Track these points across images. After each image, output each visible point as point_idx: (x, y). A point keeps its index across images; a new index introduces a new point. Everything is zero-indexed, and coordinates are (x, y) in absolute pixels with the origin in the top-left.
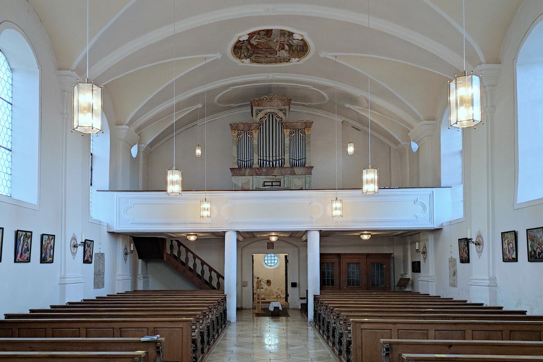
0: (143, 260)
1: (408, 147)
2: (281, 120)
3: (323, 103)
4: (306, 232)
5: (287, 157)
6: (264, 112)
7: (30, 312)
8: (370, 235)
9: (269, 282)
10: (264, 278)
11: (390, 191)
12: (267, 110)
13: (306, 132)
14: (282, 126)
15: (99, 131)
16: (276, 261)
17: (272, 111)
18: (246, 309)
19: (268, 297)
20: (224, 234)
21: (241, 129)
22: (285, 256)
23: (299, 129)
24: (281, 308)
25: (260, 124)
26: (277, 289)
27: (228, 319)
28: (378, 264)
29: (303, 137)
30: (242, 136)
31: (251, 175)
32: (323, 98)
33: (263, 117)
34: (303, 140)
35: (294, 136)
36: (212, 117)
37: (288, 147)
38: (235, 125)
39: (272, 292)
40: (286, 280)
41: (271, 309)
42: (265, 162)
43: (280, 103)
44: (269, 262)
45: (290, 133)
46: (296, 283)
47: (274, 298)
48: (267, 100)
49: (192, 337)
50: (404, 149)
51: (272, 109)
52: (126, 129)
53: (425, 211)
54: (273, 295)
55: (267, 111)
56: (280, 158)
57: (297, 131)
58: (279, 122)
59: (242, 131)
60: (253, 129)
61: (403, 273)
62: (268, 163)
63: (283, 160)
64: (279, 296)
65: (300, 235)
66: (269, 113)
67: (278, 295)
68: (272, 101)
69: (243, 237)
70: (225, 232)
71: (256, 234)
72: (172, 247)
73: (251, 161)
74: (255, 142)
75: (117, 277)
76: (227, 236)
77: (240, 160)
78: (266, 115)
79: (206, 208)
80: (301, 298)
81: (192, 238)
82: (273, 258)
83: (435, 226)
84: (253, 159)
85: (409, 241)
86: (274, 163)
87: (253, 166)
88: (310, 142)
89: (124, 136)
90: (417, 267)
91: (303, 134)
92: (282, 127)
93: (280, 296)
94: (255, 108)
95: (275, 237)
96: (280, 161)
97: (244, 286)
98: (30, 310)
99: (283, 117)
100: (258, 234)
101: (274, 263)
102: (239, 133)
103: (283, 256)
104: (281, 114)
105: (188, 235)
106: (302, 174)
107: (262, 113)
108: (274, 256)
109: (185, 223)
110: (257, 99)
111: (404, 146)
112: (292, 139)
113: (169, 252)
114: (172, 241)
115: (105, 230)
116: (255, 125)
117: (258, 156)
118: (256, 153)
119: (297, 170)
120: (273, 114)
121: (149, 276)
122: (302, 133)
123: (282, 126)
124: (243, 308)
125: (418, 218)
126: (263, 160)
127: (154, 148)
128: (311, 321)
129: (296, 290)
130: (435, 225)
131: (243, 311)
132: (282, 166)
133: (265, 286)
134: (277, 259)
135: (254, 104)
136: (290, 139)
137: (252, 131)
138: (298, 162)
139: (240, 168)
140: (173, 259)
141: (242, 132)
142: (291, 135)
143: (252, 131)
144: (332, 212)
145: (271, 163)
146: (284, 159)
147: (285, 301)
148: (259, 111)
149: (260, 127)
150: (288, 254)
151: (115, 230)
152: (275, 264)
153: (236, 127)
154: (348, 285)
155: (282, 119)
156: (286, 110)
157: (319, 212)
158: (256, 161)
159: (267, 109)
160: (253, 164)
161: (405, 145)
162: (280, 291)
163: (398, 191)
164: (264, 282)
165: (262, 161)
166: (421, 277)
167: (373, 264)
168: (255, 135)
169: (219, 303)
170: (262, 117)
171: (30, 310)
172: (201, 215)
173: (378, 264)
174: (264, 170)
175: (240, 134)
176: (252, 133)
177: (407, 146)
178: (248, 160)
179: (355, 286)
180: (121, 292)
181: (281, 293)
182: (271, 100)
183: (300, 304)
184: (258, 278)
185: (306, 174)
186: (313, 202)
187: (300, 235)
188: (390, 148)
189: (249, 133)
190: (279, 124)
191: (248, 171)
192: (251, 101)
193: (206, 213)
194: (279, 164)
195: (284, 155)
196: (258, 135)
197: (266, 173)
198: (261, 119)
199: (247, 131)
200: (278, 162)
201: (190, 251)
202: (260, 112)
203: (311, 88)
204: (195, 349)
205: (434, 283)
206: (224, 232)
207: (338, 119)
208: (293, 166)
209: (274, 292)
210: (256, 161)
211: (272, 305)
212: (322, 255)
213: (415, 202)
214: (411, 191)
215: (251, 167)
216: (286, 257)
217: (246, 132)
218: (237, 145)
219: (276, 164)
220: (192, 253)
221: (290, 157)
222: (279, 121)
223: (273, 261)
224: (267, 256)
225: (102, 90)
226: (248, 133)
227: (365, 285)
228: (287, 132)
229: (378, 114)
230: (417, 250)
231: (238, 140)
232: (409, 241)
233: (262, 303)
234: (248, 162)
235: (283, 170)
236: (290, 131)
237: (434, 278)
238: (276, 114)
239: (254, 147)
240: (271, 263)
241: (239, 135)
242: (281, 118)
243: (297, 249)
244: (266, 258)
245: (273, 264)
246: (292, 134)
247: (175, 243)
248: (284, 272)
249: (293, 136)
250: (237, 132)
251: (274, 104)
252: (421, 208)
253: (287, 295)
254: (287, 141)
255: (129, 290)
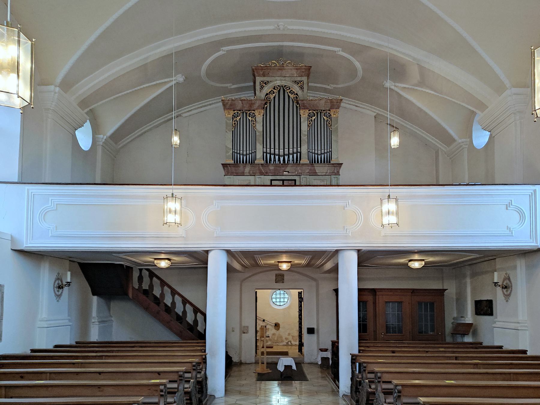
0: (102, 297)
1: (467, 146)
2: (296, 97)
3: (351, 83)
4: (337, 252)
5: (304, 149)
6: (271, 85)
7: (31, 352)
8: (424, 262)
9: (277, 326)
10: (271, 320)
11: (470, 188)
12: (276, 82)
13: (332, 114)
14: (298, 106)
15: (28, 104)
16: (286, 300)
17: (284, 83)
18: (246, 364)
19: (276, 344)
20: (206, 254)
21: (238, 108)
22: (299, 292)
23: (321, 111)
24: (294, 367)
25: (267, 101)
26: (287, 334)
27: (210, 392)
28: (426, 304)
29: (327, 121)
30: (240, 119)
31: (252, 174)
32: (353, 72)
33: (270, 92)
34: (328, 127)
35: (314, 119)
36: (201, 105)
37: (306, 135)
38: (230, 102)
39: (281, 337)
40: (299, 324)
41: (281, 368)
42: (272, 156)
43: (294, 72)
44: (278, 300)
45: (309, 116)
46: (314, 328)
47: (284, 345)
48: (277, 68)
49: (185, 390)
50: (462, 148)
51: (283, 81)
52: (56, 93)
53: (522, 222)
54: (282, 341)
55: (276, 83)
56: (294, 151)
57: (319, 114)
58: (293, 100)
59: (240, 111)
60: (255, 108)
61: (455, 315)
62: (277, 157)
63: (299, 154)
64: (289, 343)
65: (322, 263)
66: (279, 86)
67: (288, 342)
68: (285, 69)
69: (241, 265)
70: (209, 252)
71: (259, 257)
72: (140, 278)
73: (253, 154)
74: (259, 127)
75: (39, 322)
76: (211, 258)
77: (237, 153)
78: (274, 89)
79: (173, 209)
80: (322, 350)
81: (164, 264)
82: (282, 296)
83: (539, 245)
84: (256, 152)
85: (468, 273)
86: (286, 158)
87: (256, 162)
88: (337, 128)
89: (54, 103)
90: (486, 308)
91: (327, 117)
92: (297, 107)
93: (291, 343)
94: (259, 79)
95: (287, 264)
96: (295, 155)
97: (244, 333)
98: (31, 350)
99: (300, 93)
100: (261, 257)
101: (284, 302)
102: (235, 113)
103: (295, 292)
104: (296, 88)
105: (155, 259)
106: (327, 174)
107: (268, 86)
108: (284, 294)
109: (143, 238)
110: (262, 66)
111: (461, 144)
112: (312, 124)
113: (136, 286)
114: (141, 270)
115: (8, 246)
116: (258, 104)
117: (263, 148)
118: (259, 143)
119: (319, 169)
120: (283, 89)
121: (112, 319)
122: (326, 116)
123: (298, 106)
124: (242, 362)
125: (513, 231)
126: (270, 154)
127: (121, 144)
128: (344, 395)
129: (314, 337)
130: (538, 244)
131: (243, 367)
132: (297, 162)
133: (271, 331)
134: (287, 296)
135: (257, 73)
136: (310, 123)
137: (254, 112)
138: (319, 157)
139: (236, 164)
140: (142, 297)
141: (239, 112)
142: (311, 119)
143: (254, 112)
144: (382, 219)
145: (282, 159)
146: (300, 153)
147: (299, 352)
148: (265, 83)
149: (266, 106)
150: (302, 290)
151: (25, 245)
152: (285, 303)
153: (231, 105)
154: (387, 333)
155: (298, 96)
156: (303, 83)
157: (358, 220)
158: (259, 155)
159: (276, 80)
160: (255, 159)
161: (463, 142)
162: (291, 337)
163: (482, 190)
164: (272, 326)
165: (268, 155)
166: (497, 323)
167: (420, 303)
168: (259, 118)
169: (180, 378)
170: (268, 92)
171: (31, 350)
172: (164, 221)
173: (426, 304)
174: (272, 168)
175: (238, 116)
176: (254, 114)
177: (465, 145)
178: (248, 152)
179: (396, 334)
180: (44, 347)
181: (293, 339)
182: (281, 68)
183: (320, 359)
184: (264, 321)
185: (332, 174)
186: (348, 206)
187: (322, 263)
188: (437, 153)
189: (249, 114)
190: (293, 102)
191: (247, 169)
192: (253, 68)
193: (171, 218)
194: (293, 160)
195: (300, 147)
196: (263, 118)
197: (274, 172)
198: (267, 94)
199: (247, 112)
200: (291, 156)
201: (166, 284)
202: (266, 84)
203: (339, 53)
204: (189, 402)
205: (527, 332)
206: (207, 252)
207: (370, 112)
208: (313, 162)
209: (284, 338)
210: (259, 155)
211: (281, 362)
212: (360, 290)
213: (508, 205)
214: (501, 190)
215: (252, 162)
216: (300, 294)
217: (246, 113)
218: (233, 131)
219: (288, 160)
220: (170, 287)
221: (309, 150)
222: (294, 98)
223: (282, 300)
224: (275, 293)
225: (32, 44)
226: (248, 114)
227: (410, 332)
228: (304, 114)
229: (433, 92)
230: (496, 283)
231: (233, 124)
232: (468, 273)
233: (269, 353)
234: (248, 156)
235: (298, 168)
236: (309, 113)
237: (526, 325)
238: (290, 89)
239: (257, 134)
240: (280, 302)
241: (235, 116)
242: (297, 94)
243: (314, 283)
244: (274, 296)
245: (283, 303)
246: (312, 117)
247: (146, 274)
248: (297, 314)
249: (313, 119)
250: (232, 113)
251: (286, 74)
252: (517, 216)
253: (301, 345)
254: (304, 127)
255: (67, 341)
